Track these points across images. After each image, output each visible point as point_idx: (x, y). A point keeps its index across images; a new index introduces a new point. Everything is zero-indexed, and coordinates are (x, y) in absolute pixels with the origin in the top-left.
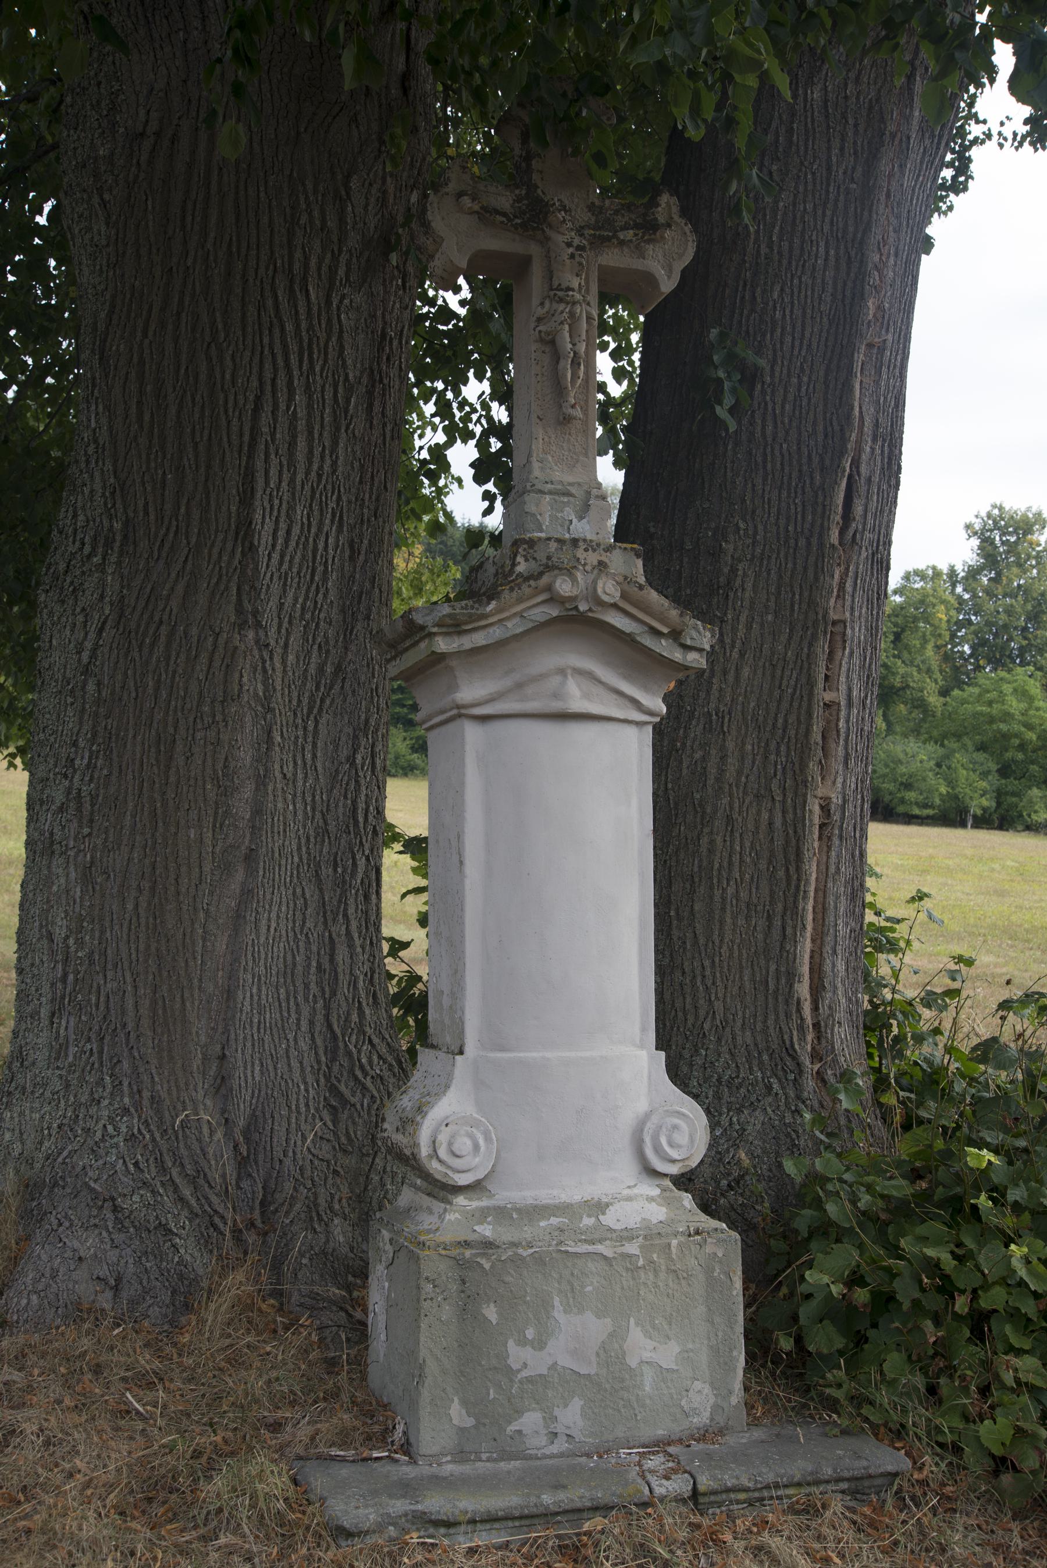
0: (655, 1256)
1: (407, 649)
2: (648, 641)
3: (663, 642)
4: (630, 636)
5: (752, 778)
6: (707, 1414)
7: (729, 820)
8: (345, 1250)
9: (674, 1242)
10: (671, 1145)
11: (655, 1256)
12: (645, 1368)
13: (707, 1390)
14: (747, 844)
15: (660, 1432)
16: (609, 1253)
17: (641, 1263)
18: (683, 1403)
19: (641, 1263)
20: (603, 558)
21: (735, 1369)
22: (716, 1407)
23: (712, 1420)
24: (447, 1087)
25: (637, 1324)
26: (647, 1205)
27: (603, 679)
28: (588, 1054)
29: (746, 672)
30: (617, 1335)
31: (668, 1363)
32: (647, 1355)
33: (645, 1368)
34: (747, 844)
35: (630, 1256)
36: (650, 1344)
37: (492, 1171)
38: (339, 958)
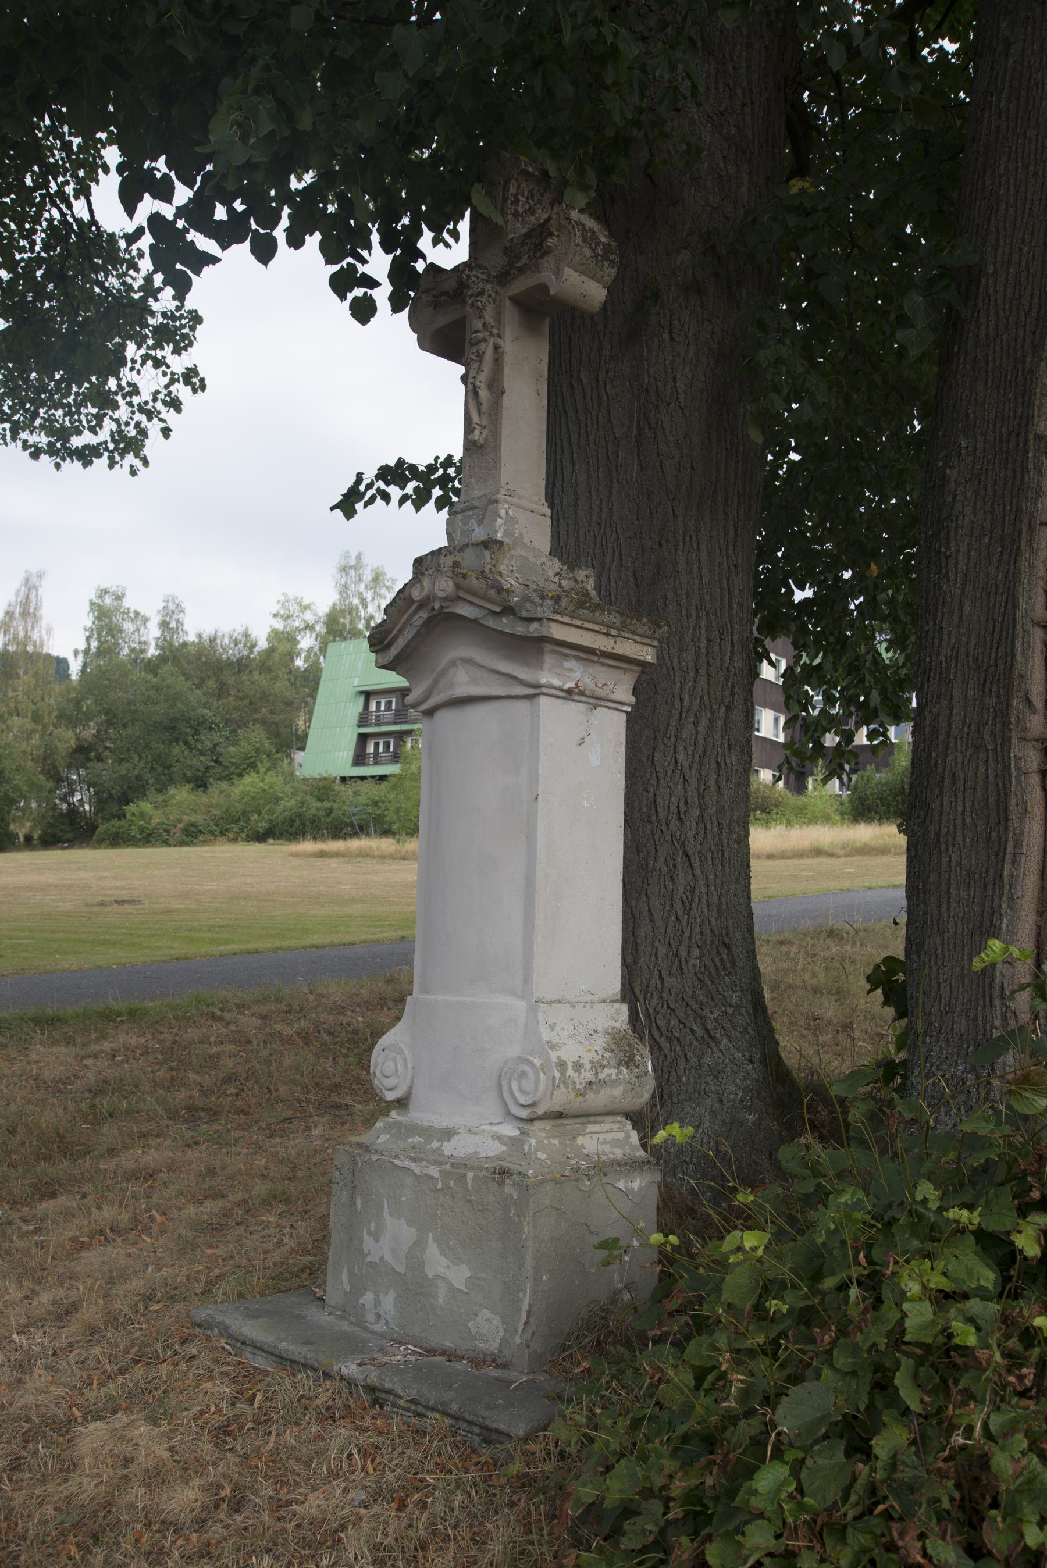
0: (452, 1183)
1: (603, 664)
2: (490, 622)
3: (504, 620)
4: (475, 621)
5: (973, 728)
6: (497, 1345)
7: (954, 777)
8: (365, 1138)
9: (470, 1175)
10: (522, 1091)
11: (452, 1183)
12: (440, 1282)
13: (497, 1321)
14: (968, 804)
15: (447, 1343)
16: (417, 1171)
17: (440, 1186)
18: (470, 1324)
19: (440, 1186)
20: (458, 559)
21: (520, 1310)
22: (504, 1342)
23: (500, 1351)
24: (398, 1019)
25: (434, 1240)
26: (490, 1141)
27: (482, 663)
28: (468, 999)
29: (967, 610)
30: (419, 1244)
31: (460, 1284)
32: (441, 1270)
33: (440, 1282)
34: (968, 804)
35: (433, 1178)
36: (444, 1261)
37: (411, 1088)
38: (641, 933)
